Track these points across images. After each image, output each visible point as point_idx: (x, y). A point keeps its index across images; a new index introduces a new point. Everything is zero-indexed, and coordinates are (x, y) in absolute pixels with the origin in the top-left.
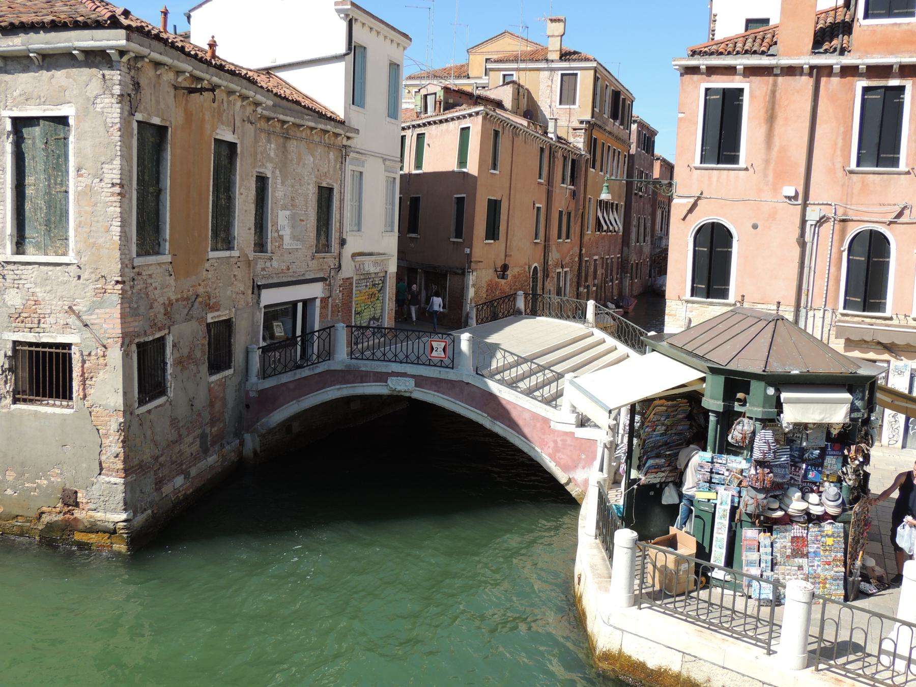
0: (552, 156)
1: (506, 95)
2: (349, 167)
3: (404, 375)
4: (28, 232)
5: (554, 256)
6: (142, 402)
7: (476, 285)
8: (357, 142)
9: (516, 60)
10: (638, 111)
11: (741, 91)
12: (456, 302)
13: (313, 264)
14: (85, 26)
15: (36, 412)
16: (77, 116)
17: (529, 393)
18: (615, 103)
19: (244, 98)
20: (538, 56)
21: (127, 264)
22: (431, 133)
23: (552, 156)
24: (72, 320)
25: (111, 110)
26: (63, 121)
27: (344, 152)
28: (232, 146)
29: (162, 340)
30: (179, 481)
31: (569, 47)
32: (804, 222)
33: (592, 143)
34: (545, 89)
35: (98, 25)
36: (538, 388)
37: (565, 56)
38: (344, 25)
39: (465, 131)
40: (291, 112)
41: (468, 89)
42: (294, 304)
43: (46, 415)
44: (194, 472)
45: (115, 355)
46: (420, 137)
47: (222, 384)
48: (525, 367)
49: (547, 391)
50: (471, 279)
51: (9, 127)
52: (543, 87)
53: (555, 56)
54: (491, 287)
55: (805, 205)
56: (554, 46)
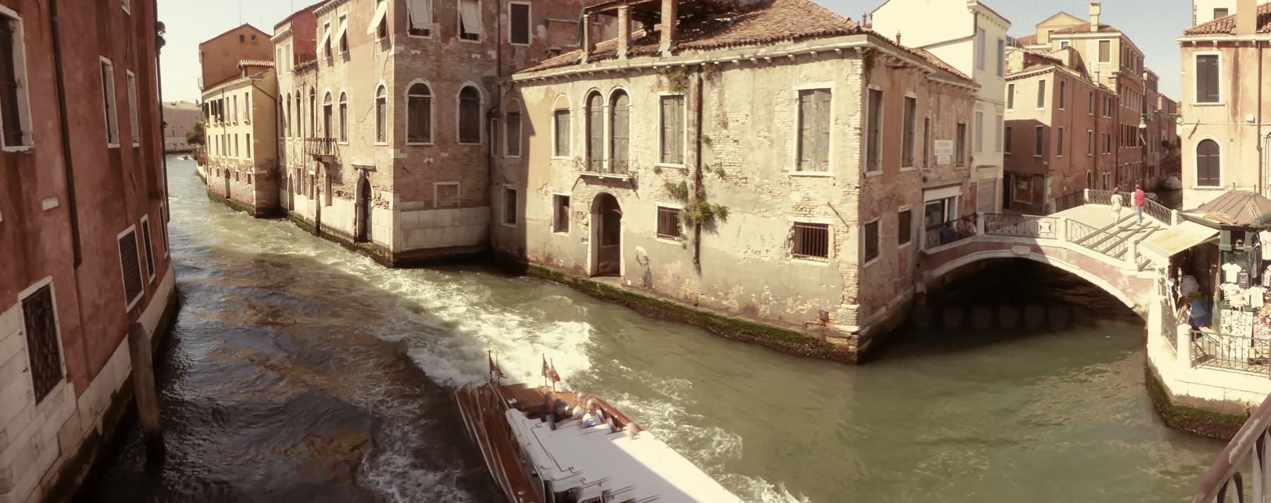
0: (1097, 98)
1: (1064, 57)
2: (975, 110)
3: (1024, 244)
4: (804, 158)
5: (1101, 164)
6: (867, 260)
7: (1050, 186)
8: (981, 93)
9: (1069, 31)
10: (1147, 64)
11: (1216, 57)
12: (1039, 196)
13: (954, 174)
14: (843, 34)
15: (806, 265)
16: (837, 89)
17: (1104, 252)
18: (1130, 57)
19: (920, 70)
20: (1084, 29)
21: (863, 176)
22: (1018, 84)
23: (1097, 98)
24: (829, 210)
25: (856, 82)
26: (828, 91)
27: (972, 100)
28: (913, 100)
29: (876, 223)
30: (883, 310)
31: (1104, 23)
32: (1259, 136)
33: (1119, 86)
34: (1089, 51)
35: (850, 33)
36: (1107, 250)
37: (1101, 28)
38: (972, 16)
39: (1042, 83)
40: (946, 78)
41: (1038, 52)
42: (943, 201)
43: (812, 267)
44: (891, 305)
45: (854, 231)
46: (1011, 87)
47: (905, 250)
48: (1102, 236)
49: (1118, 250)
50: (1049, 181)
51: (797, 96)
52: (1088, 50)
53: (1094, 29)
54: (1061, 185)
55: (1259, 126)
56: (1094, 21)
